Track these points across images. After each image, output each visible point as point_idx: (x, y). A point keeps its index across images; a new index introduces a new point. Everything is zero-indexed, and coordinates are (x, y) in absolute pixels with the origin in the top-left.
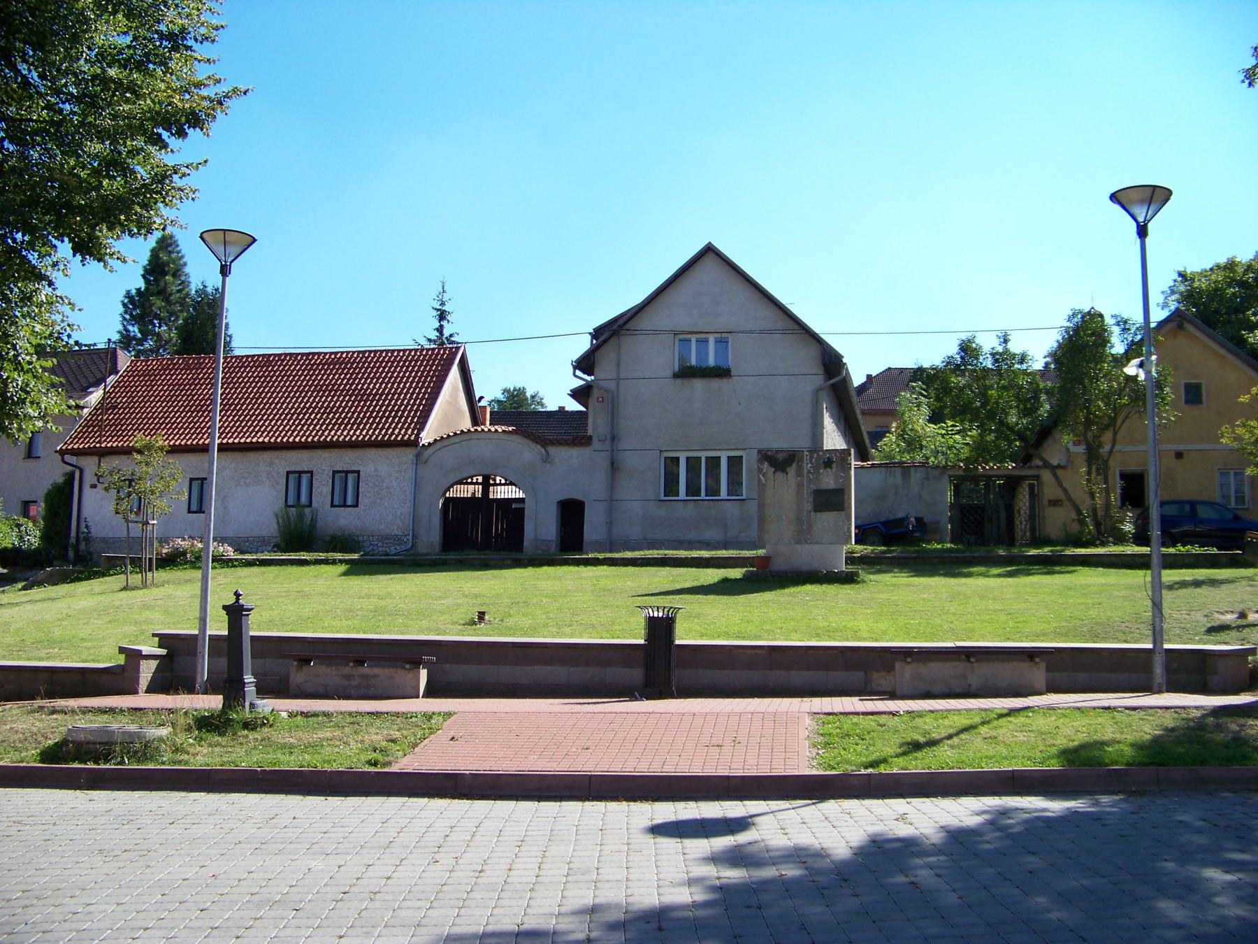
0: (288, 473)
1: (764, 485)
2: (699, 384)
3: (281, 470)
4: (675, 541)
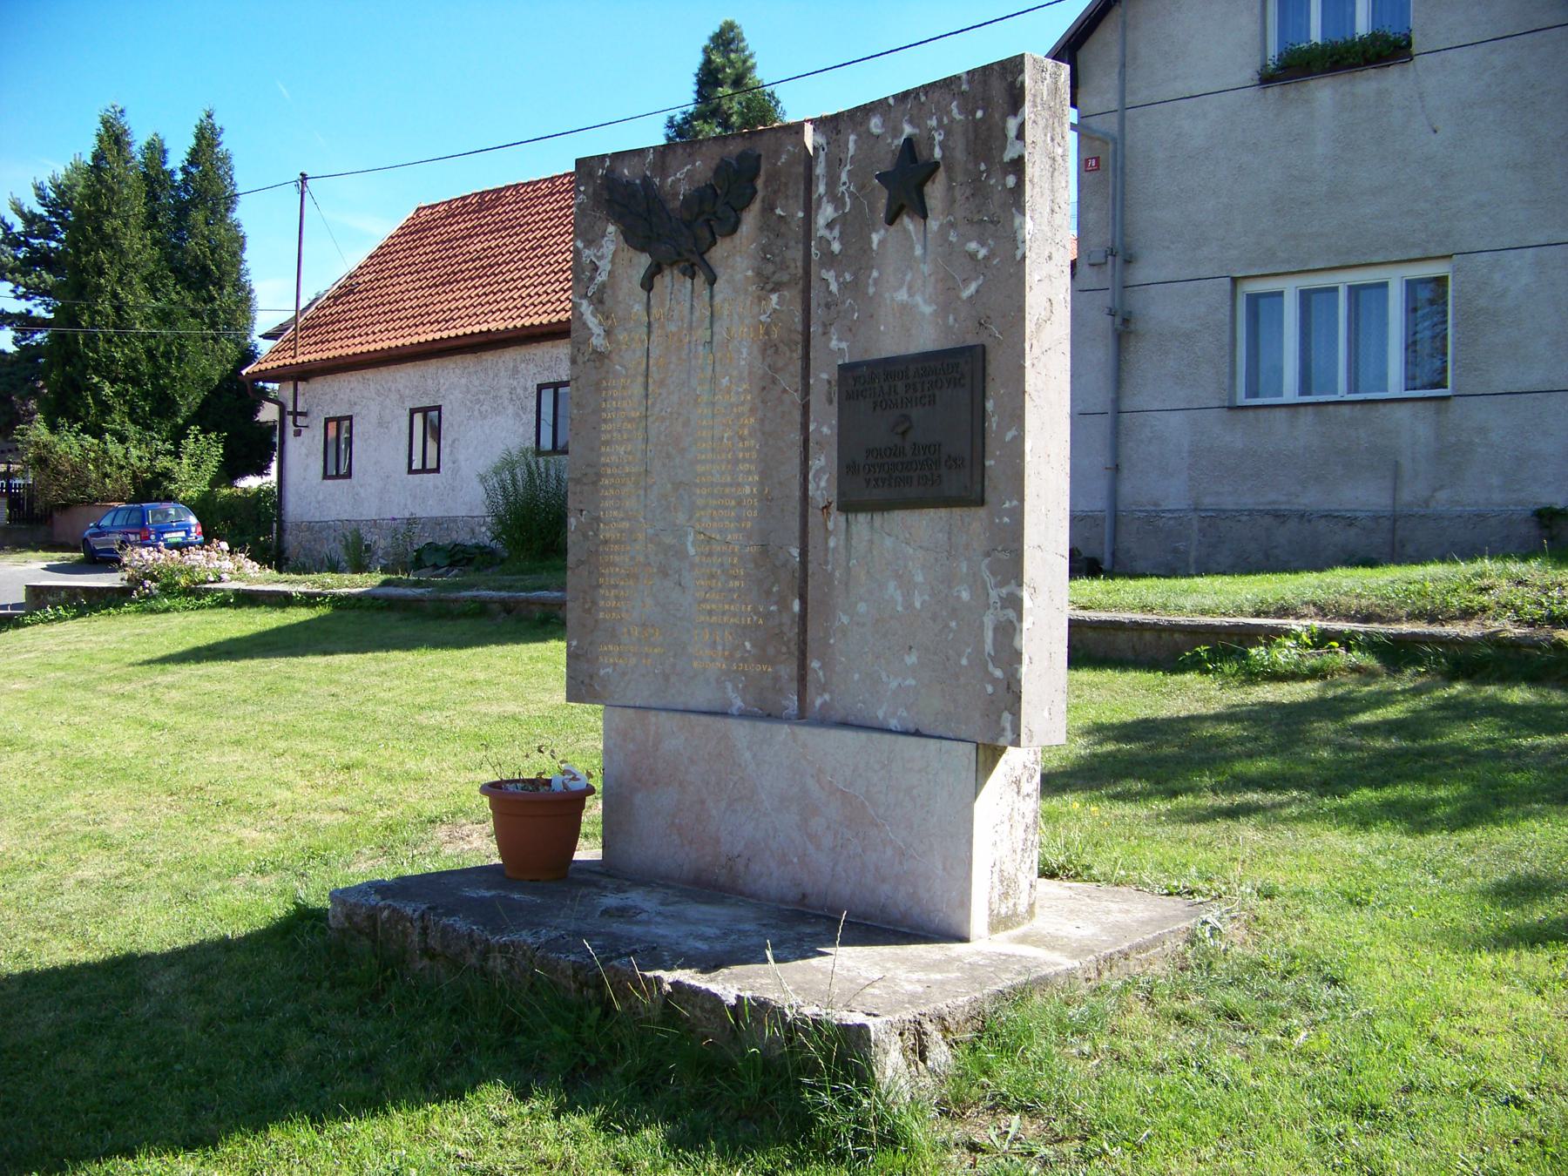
0: (541, 387)
1: (600, 356)
2: (1324, 92)
3: (529, 384)
4: (1268, 513)
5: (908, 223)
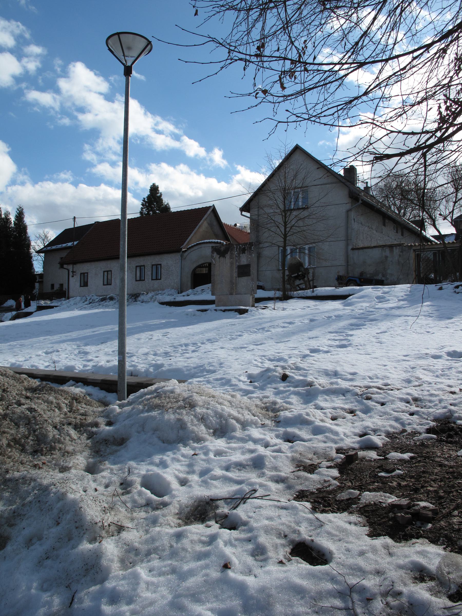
0: (137, 267)
5: (244, 254)
